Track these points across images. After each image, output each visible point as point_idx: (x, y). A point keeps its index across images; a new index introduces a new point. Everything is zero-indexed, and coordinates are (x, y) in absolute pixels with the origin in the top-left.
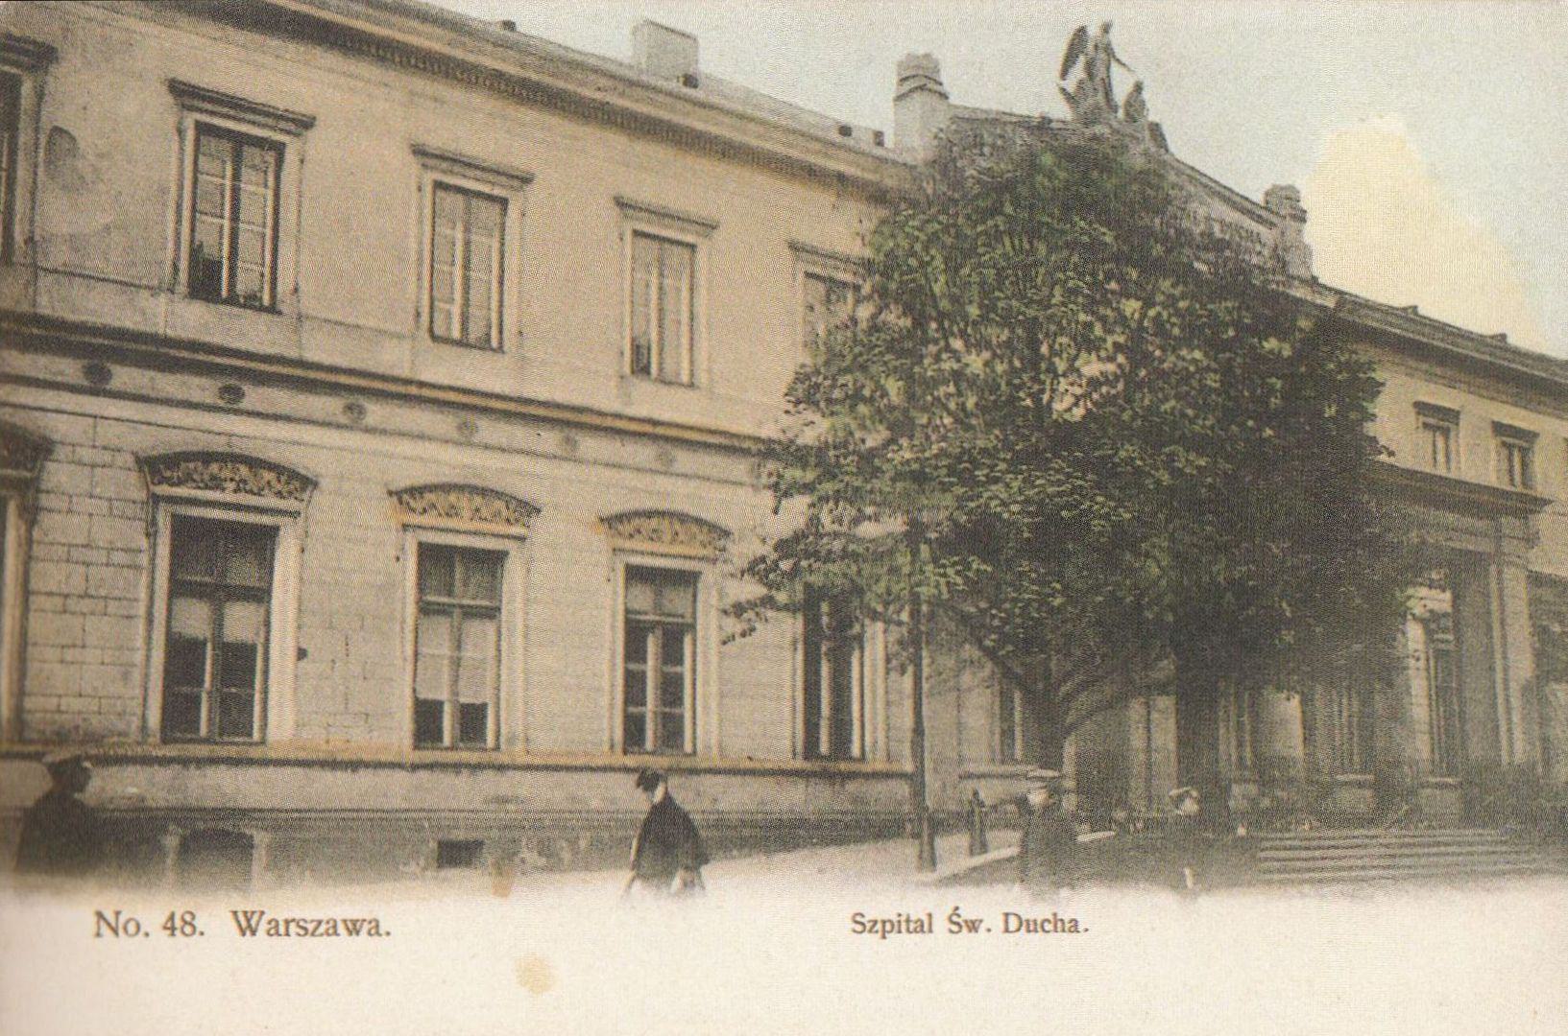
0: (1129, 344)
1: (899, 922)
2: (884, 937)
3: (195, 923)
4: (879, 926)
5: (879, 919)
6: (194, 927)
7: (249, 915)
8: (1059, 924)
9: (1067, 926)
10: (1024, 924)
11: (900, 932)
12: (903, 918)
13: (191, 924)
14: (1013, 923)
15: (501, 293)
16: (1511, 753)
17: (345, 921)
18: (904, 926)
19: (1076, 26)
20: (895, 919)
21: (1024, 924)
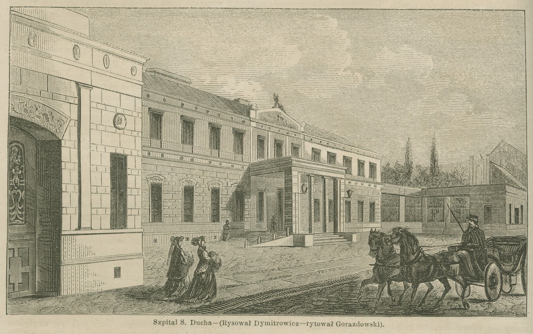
0: (399, 244)
1: (167, 322)
2: (163, 325)
3: (184, 322)
4: (162, 322)
5: (162, 321)
6: (184, 323)
7: (312, 323)
8: (206, 323)
9: (208, 323)
10: (196, 323)
11: (167, 324)
12: (168, 321)
13: (155, 322)
14: (193, 323)
15: (120, 260)
16: (340, 230)
17: (284, 322)
18: (168, 323)
19: (181, 188)
20: (166, 321)
21: (196, 323)
